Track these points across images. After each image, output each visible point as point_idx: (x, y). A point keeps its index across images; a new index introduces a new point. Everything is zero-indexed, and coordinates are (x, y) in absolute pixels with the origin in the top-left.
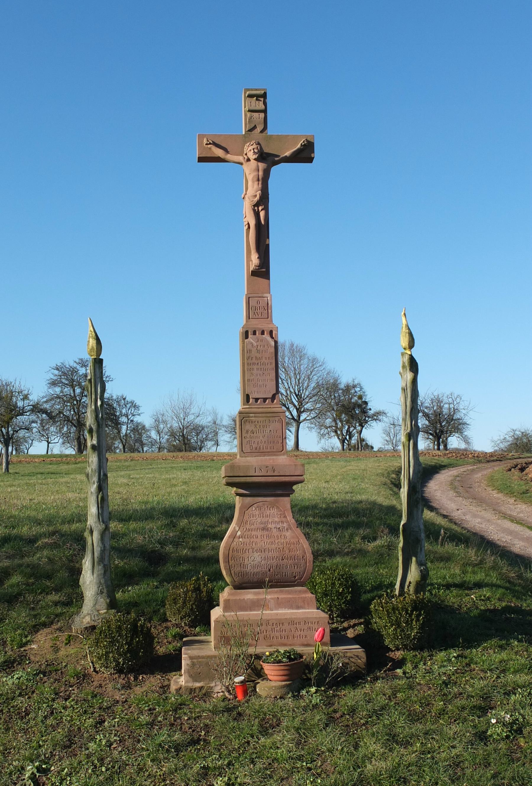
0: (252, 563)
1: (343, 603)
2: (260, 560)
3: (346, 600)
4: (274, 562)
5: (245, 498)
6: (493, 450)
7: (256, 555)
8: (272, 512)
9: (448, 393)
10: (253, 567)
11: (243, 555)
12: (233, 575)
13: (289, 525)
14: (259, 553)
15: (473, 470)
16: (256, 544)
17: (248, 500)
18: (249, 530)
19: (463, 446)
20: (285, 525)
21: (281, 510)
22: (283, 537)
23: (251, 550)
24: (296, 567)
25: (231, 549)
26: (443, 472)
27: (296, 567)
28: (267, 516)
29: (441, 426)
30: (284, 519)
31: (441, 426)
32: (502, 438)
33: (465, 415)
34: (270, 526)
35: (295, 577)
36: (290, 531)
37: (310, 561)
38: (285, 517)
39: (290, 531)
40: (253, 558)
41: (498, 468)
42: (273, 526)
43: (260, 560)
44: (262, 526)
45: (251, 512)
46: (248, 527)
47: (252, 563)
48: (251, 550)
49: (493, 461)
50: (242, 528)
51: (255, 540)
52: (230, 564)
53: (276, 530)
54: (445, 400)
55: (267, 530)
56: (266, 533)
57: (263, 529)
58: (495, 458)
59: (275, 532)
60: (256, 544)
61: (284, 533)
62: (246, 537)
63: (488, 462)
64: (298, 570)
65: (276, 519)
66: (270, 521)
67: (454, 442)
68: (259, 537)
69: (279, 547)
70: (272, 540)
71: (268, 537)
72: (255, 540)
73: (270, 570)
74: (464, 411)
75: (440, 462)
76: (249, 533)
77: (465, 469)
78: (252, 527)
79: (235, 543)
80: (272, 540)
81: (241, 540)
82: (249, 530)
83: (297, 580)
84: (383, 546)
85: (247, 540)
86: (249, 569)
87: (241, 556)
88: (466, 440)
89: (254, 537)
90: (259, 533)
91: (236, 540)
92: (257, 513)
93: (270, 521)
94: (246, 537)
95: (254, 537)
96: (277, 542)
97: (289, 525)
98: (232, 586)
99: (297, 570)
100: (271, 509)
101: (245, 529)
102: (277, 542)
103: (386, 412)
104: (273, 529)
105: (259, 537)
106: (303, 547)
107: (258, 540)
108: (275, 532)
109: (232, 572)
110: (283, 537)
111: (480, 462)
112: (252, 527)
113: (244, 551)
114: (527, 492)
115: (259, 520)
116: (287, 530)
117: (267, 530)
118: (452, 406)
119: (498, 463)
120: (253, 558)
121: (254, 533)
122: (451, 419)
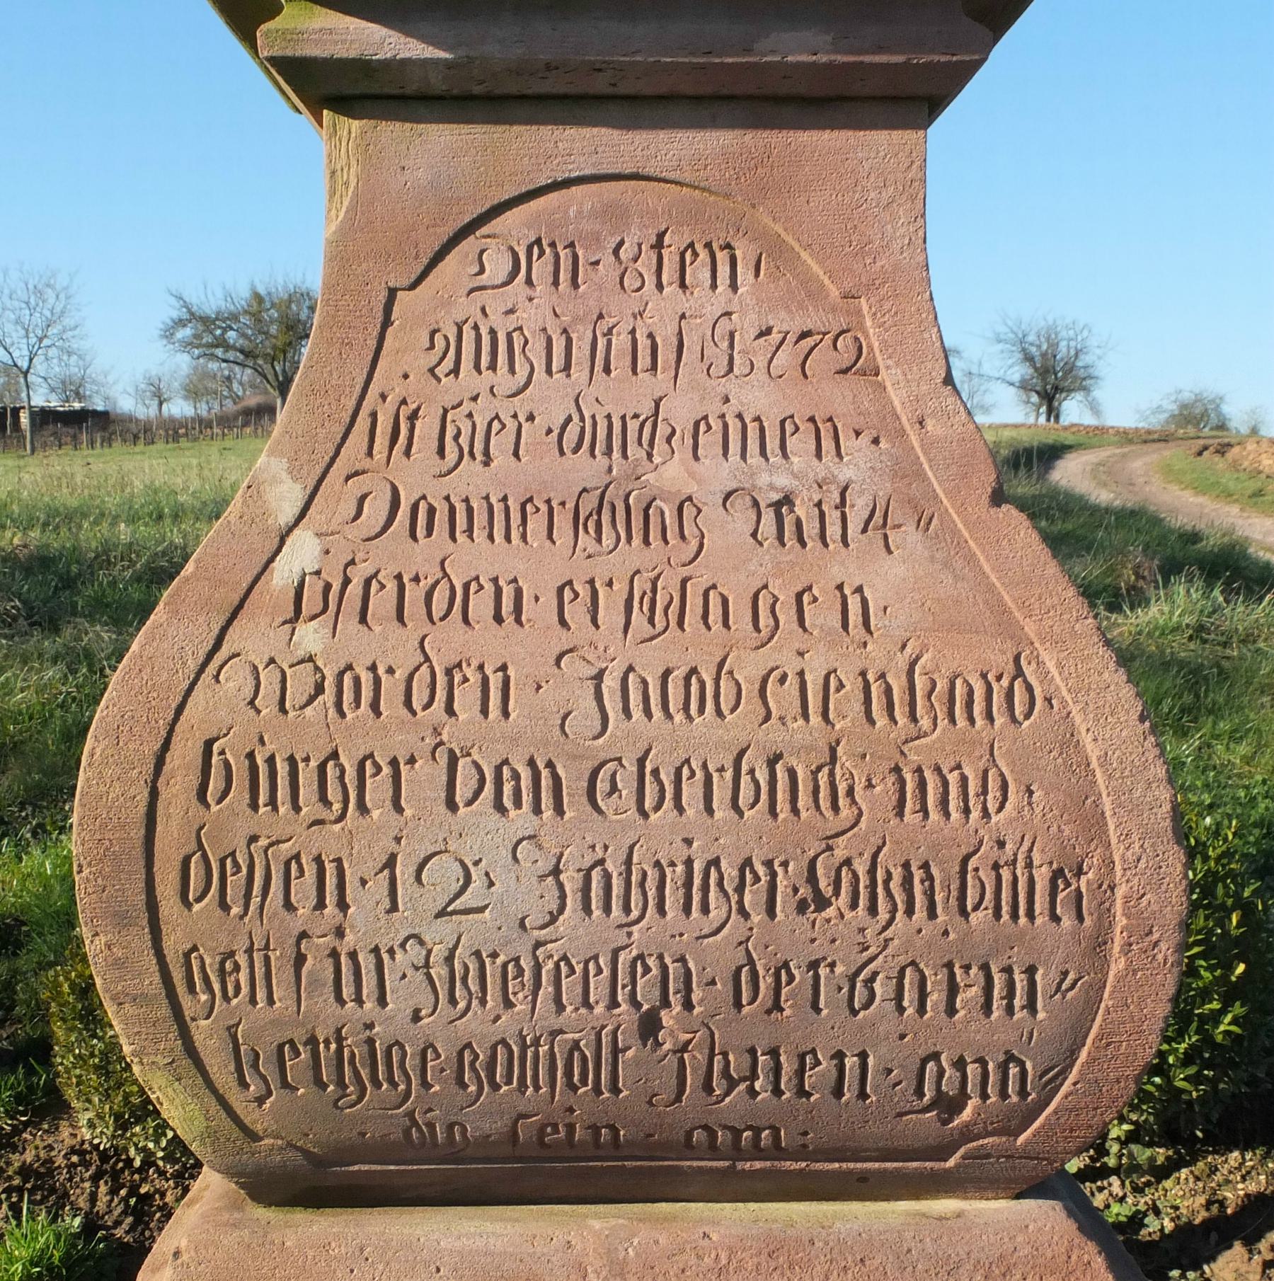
0: (439, 934)
1: (1187, 1060)
2: (533, 900)
3: (1207, 1040)
4: (709, 941)
5: (391, 132)
6: (1133, 426)
7: (485, 833)
8: (707, 302)
9: (1068, 321)
10: (457, 981)
11: (329, 841)
12: (223, 1075)
13: (906, 471)
14: (521, 820)
15: (1124, 456)
16: (497, 692)
17: (440, 157)
18: (422, 519)
19: (1089, 420)
20: (857, 465)
21: (814, 293)
22: (822, 616)
23: (424, 779)
24: (970, 995)
25: (184, 754)
26: (1069, 456)
27: (970, 995)
28: (647, 357)
29: (1056, 378)
30: (840, 398)
31: (1056, 378)
32: (1155, 406)
33: (1100, 358)
34: (671, 473)
35: (949, 1105)
36: (907, 537)
37: (1142, 930)
38: (858, 367)
39: (907, 537)
40: (443, 873)
41: (1169, 453)
42: (718, 472)
43: (533, 900)
44: (586, 470)
45: (466, 308)
46: (416, 475)
47: (439, 934)
48: (424, 779)
49: (1153, 441)
50: (337, 500)
51: (485, 642)
52: (173, 944)
53: (741, 519)
54: (1064, 334)
55: (641, 520)
56: (620, 560)
57: (592, 514)
58: (1156, 436)
59: (733, 555)
60: (497, 692)
61: (841, 567)
62: (382, 602)
63: (1145, 442)
64: (996, 1033)
65: (757, 397)
66: (679, 411)
67: (1073, 410)
68: (540, 611)
69: (773, 736)
70: (691, 647)
71: (647, 606)
72: (485, 642)
73: (649, 1026)
74: (1098, 351)
75: (1061, 439)
76: (421, 556)
77: (1108, 453)
78: (471, 480)
79: (235, 680)
80: (691, 647)
81: (310, 636)
82: (422, 519)
83: (967, 1134)
84: (1176, 629)
85: (388, 645)
86: (402, 1009)
87: (310, 843)
88: (1095, 408)
89: (481, 605)
90: (538, 563)
91: (254, 638)
92: (533, 316)
93: (679, 411)
94: (382, 602)
95: (481, 605)
96: (748, 669)
97: (906, 471)
98: (229, 1172)
99: (977, 1031)
100: (699, 272)
101: (376, 511)
102: (748, 669)
103: (961, 349)
104: (714, 511)
105: (540, 611)
106: (1070, 741)
107: (522, 649)
108: (733, 555)
109: (202, 1031)
110: (822, 616)
111: (1131, 442)
112: (471, 480)
113: (343, 785)
114: (1259, 493)
115: (551, 400)
116: (879, 521)
117: (641, 520)
118: (1073, 344)
119: (1162, 445)
120: (443, 873)
121: (476, 557)
122: (1070, 368)
